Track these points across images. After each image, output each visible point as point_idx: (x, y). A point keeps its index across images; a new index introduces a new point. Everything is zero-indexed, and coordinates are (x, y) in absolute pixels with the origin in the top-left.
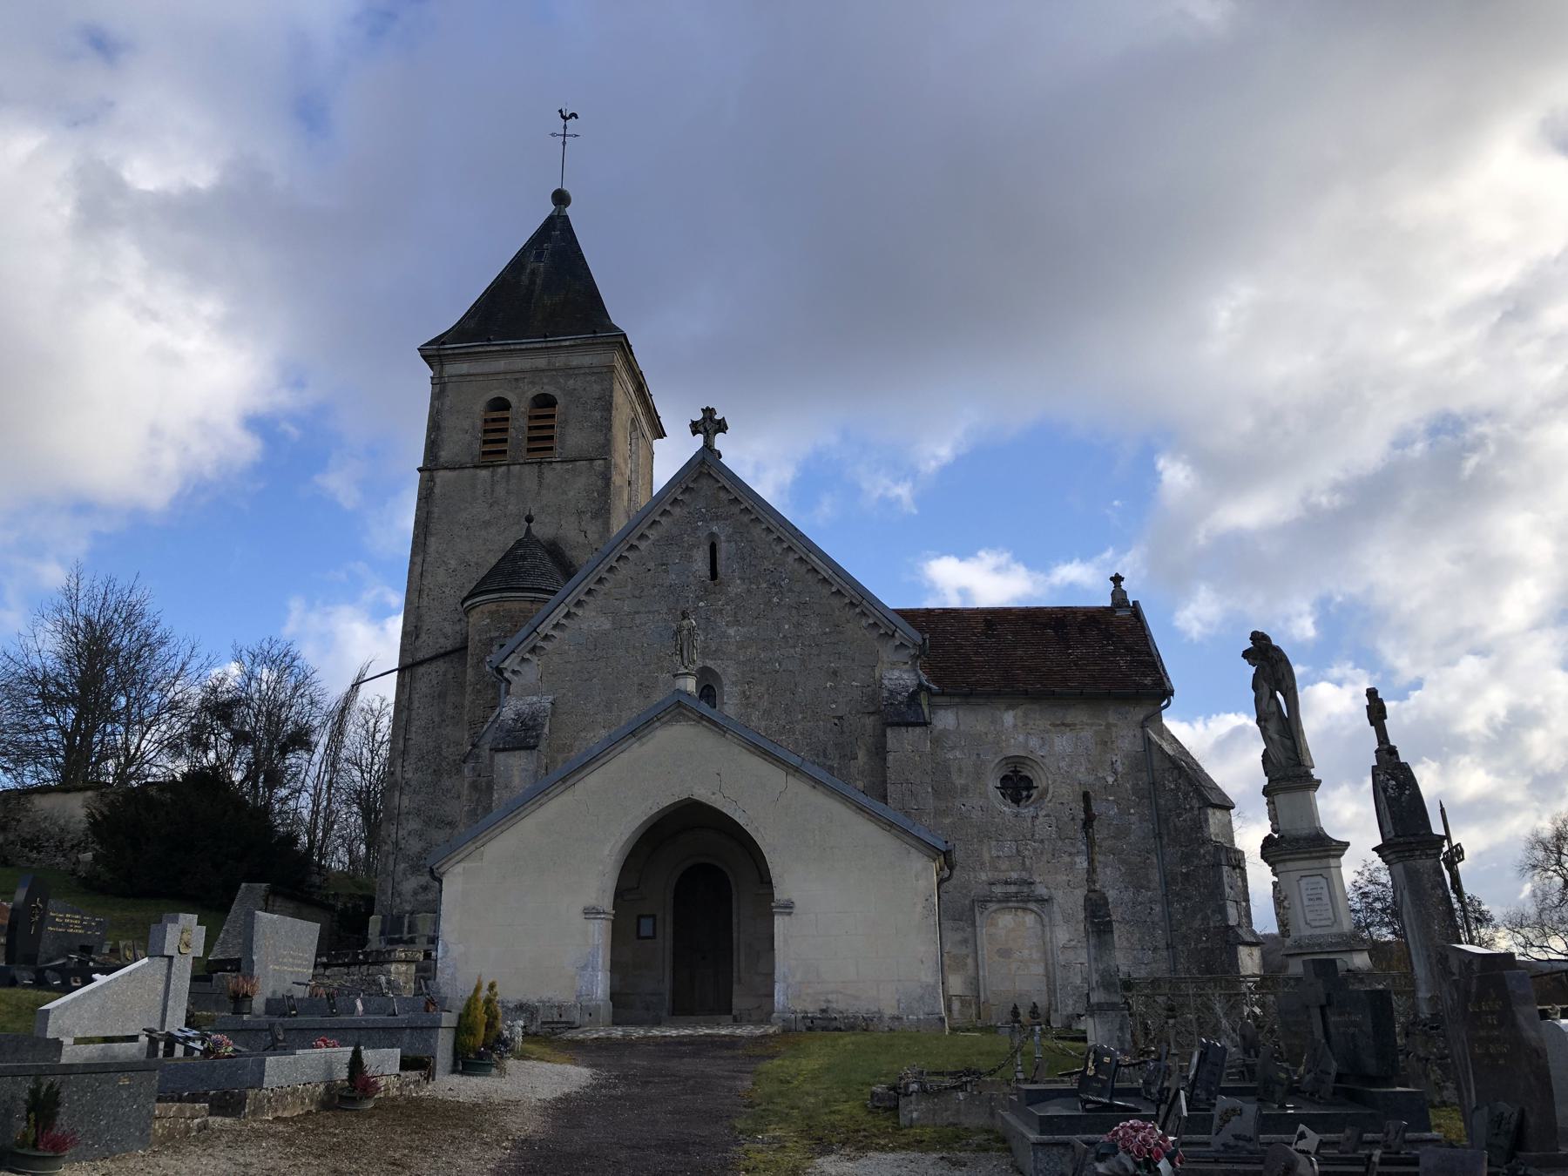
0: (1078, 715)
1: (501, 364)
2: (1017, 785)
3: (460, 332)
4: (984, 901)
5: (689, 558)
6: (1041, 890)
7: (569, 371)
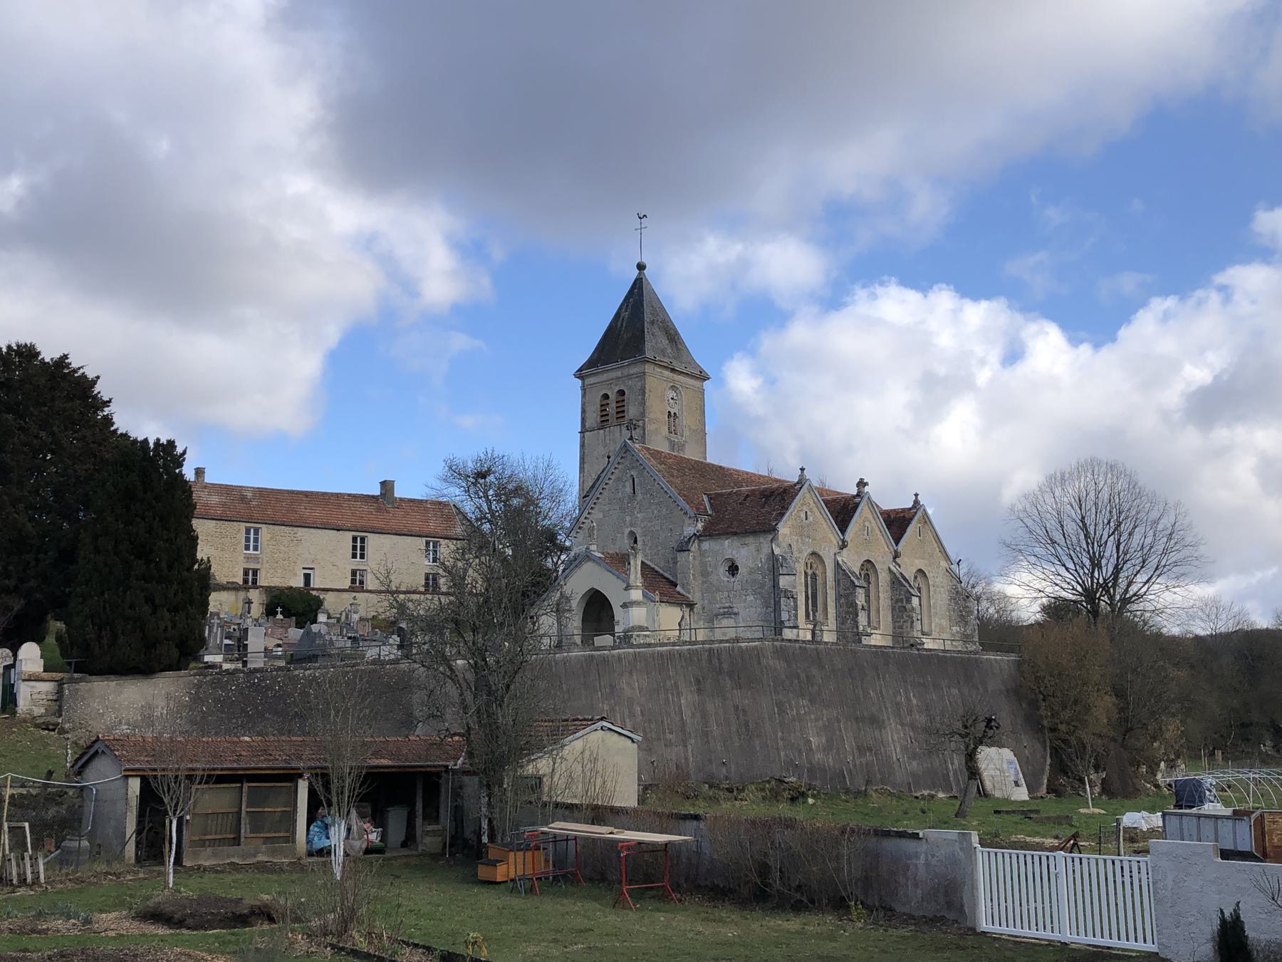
0: (750, 540)
1: (605, 377)
2: (733, 569)
3: (591, 363)
4: (717, 615)
5: (624, 486)
6: (736, 610)
7: (629, 377)
